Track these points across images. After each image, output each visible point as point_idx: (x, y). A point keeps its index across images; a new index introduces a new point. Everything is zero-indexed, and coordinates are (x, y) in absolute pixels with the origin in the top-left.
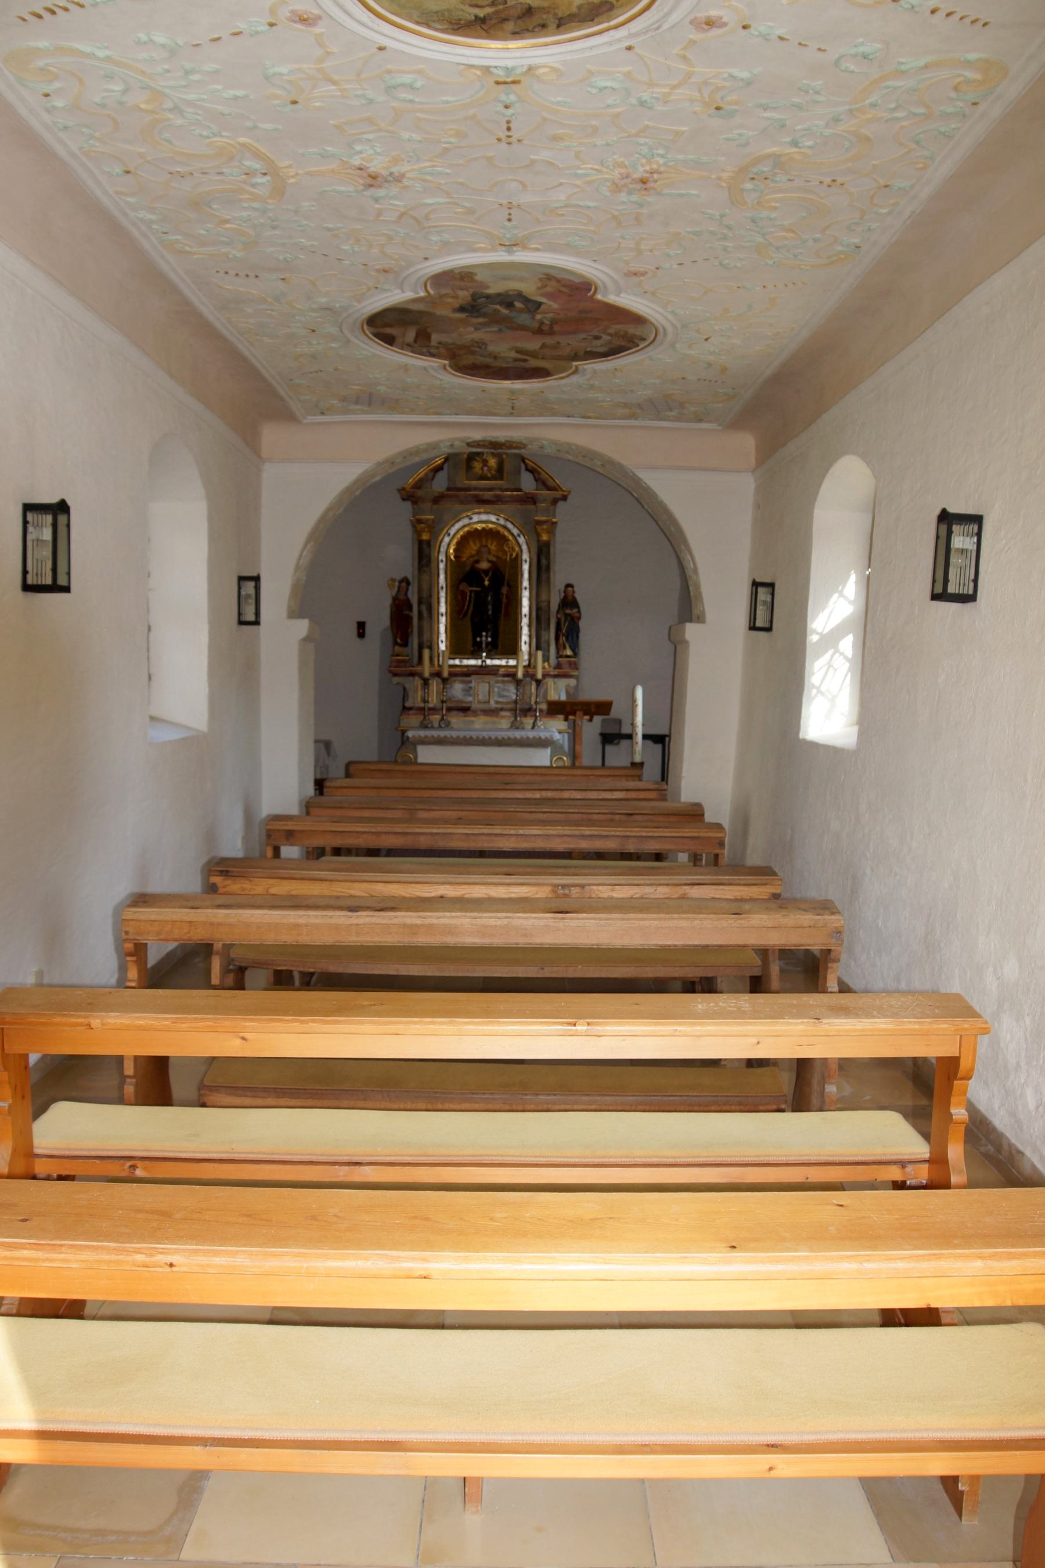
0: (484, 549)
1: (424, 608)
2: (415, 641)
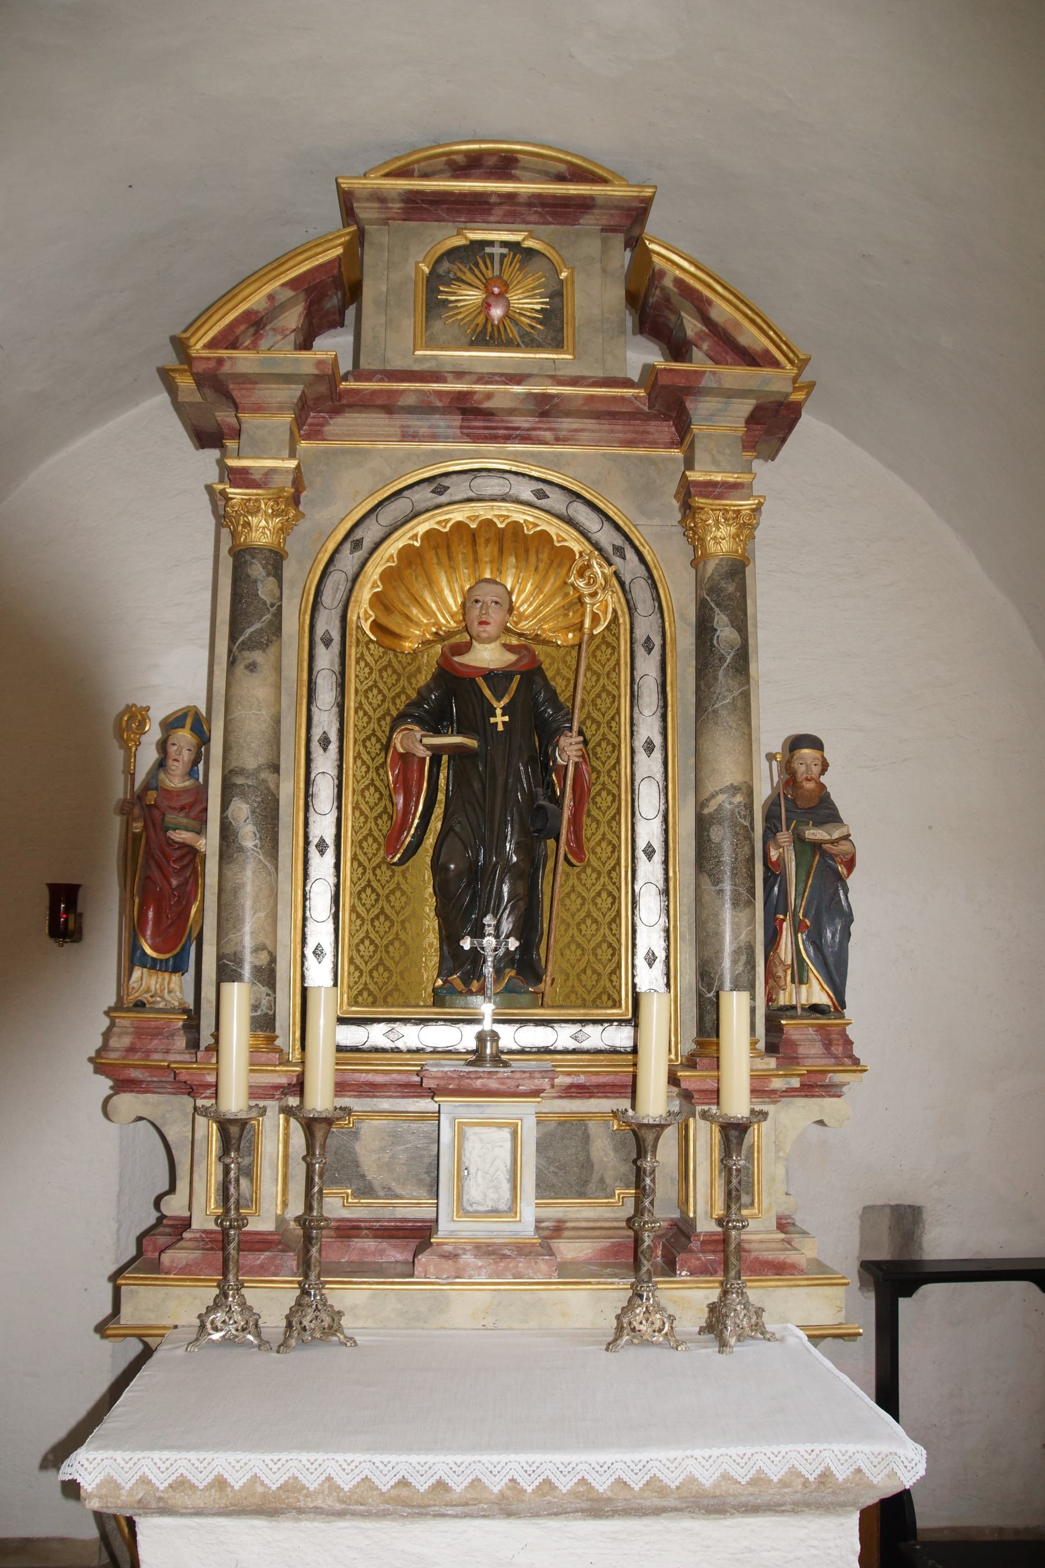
0: (488, 594)
1: (241, 810)
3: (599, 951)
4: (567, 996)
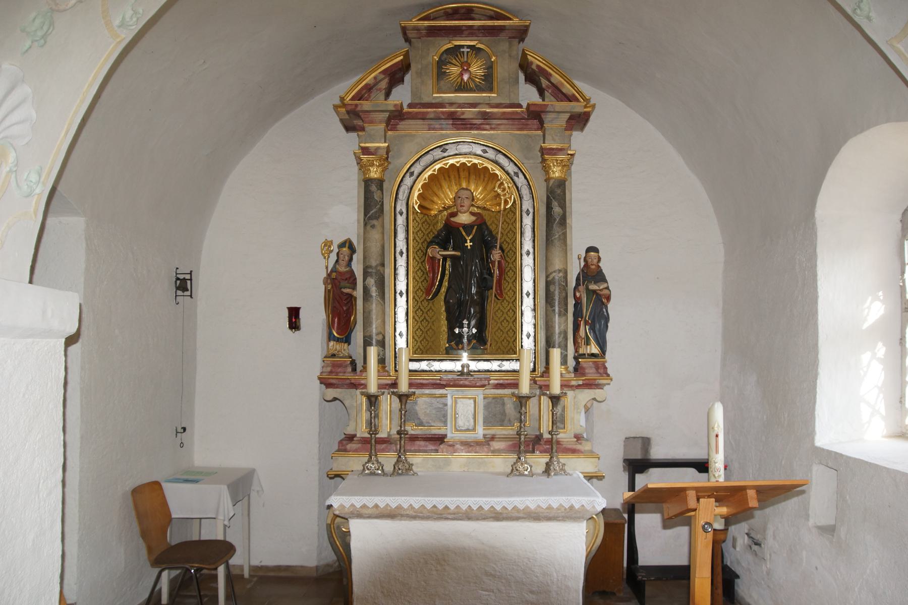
0: (464, 194)
1: (371, 281)
2: (358, 336)
3: (509, 333)
4: (497, 350)
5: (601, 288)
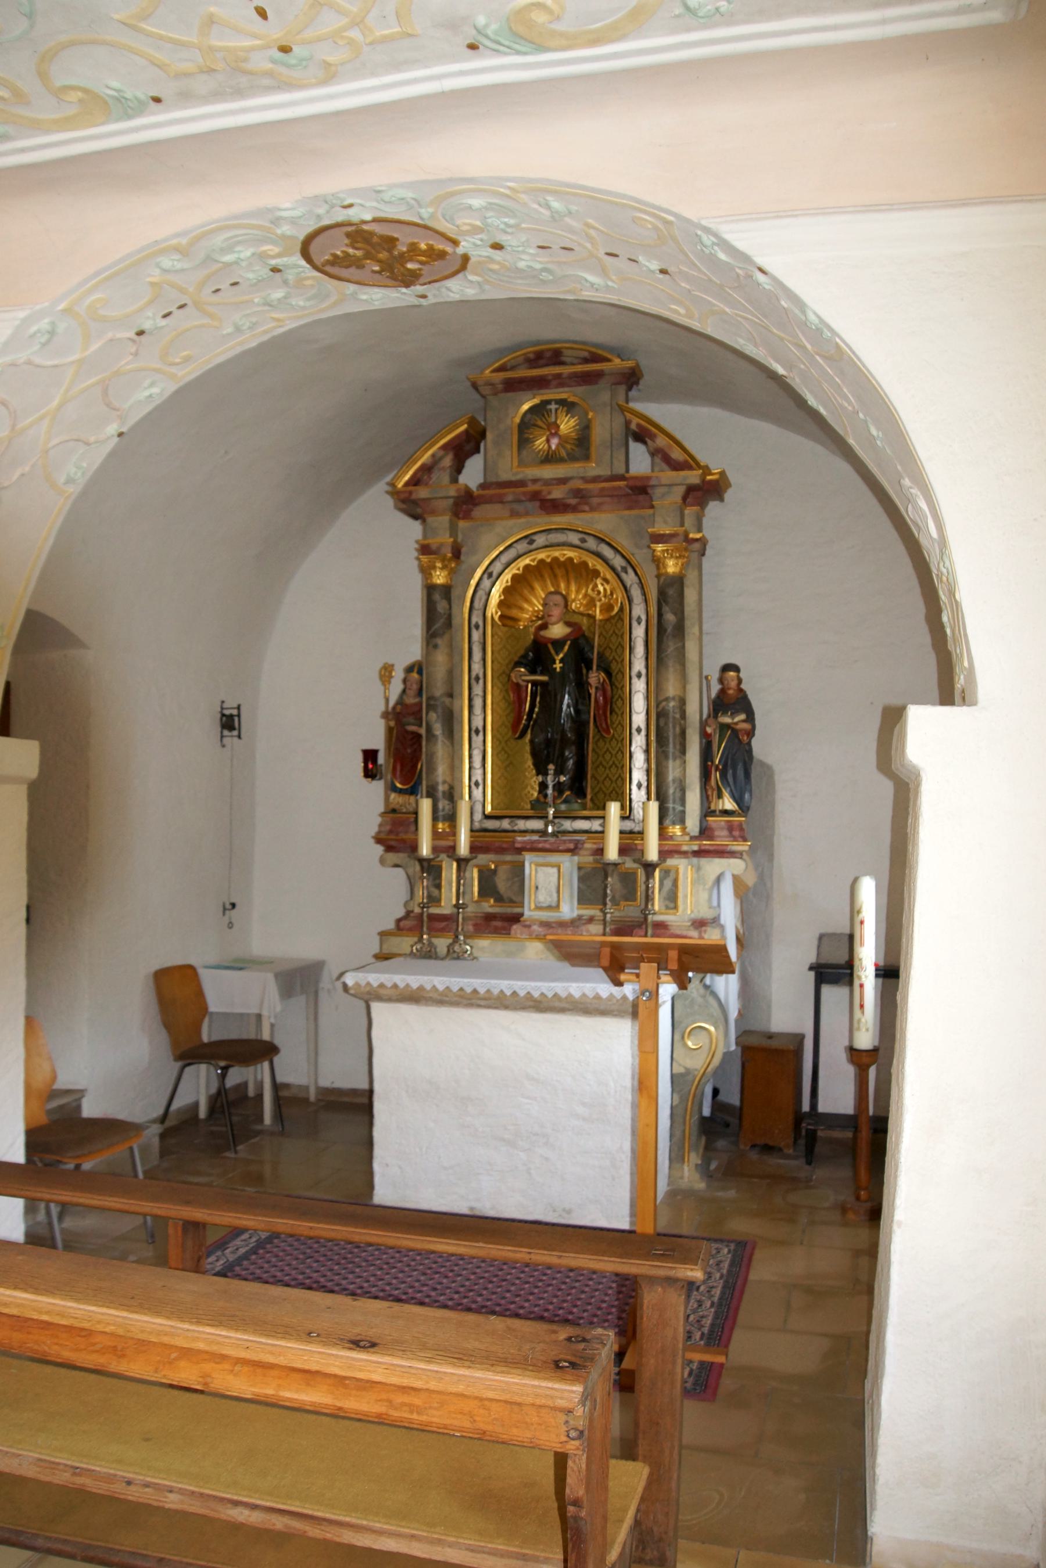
5: (736, 719)
